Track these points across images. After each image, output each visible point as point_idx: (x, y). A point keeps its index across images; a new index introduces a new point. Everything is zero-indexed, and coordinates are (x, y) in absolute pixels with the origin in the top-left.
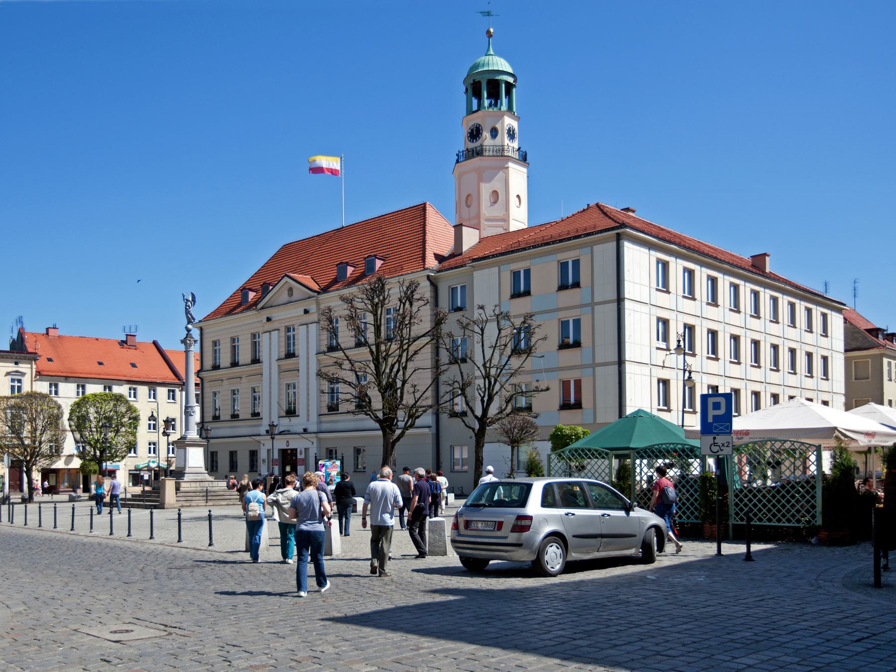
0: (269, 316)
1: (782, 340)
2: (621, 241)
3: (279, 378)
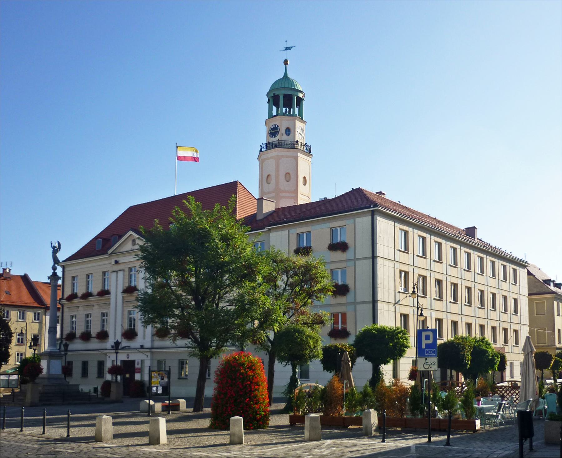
0: (117, 259)
1: (486, 287)
2: (375, 216)
3: (123, 307)
